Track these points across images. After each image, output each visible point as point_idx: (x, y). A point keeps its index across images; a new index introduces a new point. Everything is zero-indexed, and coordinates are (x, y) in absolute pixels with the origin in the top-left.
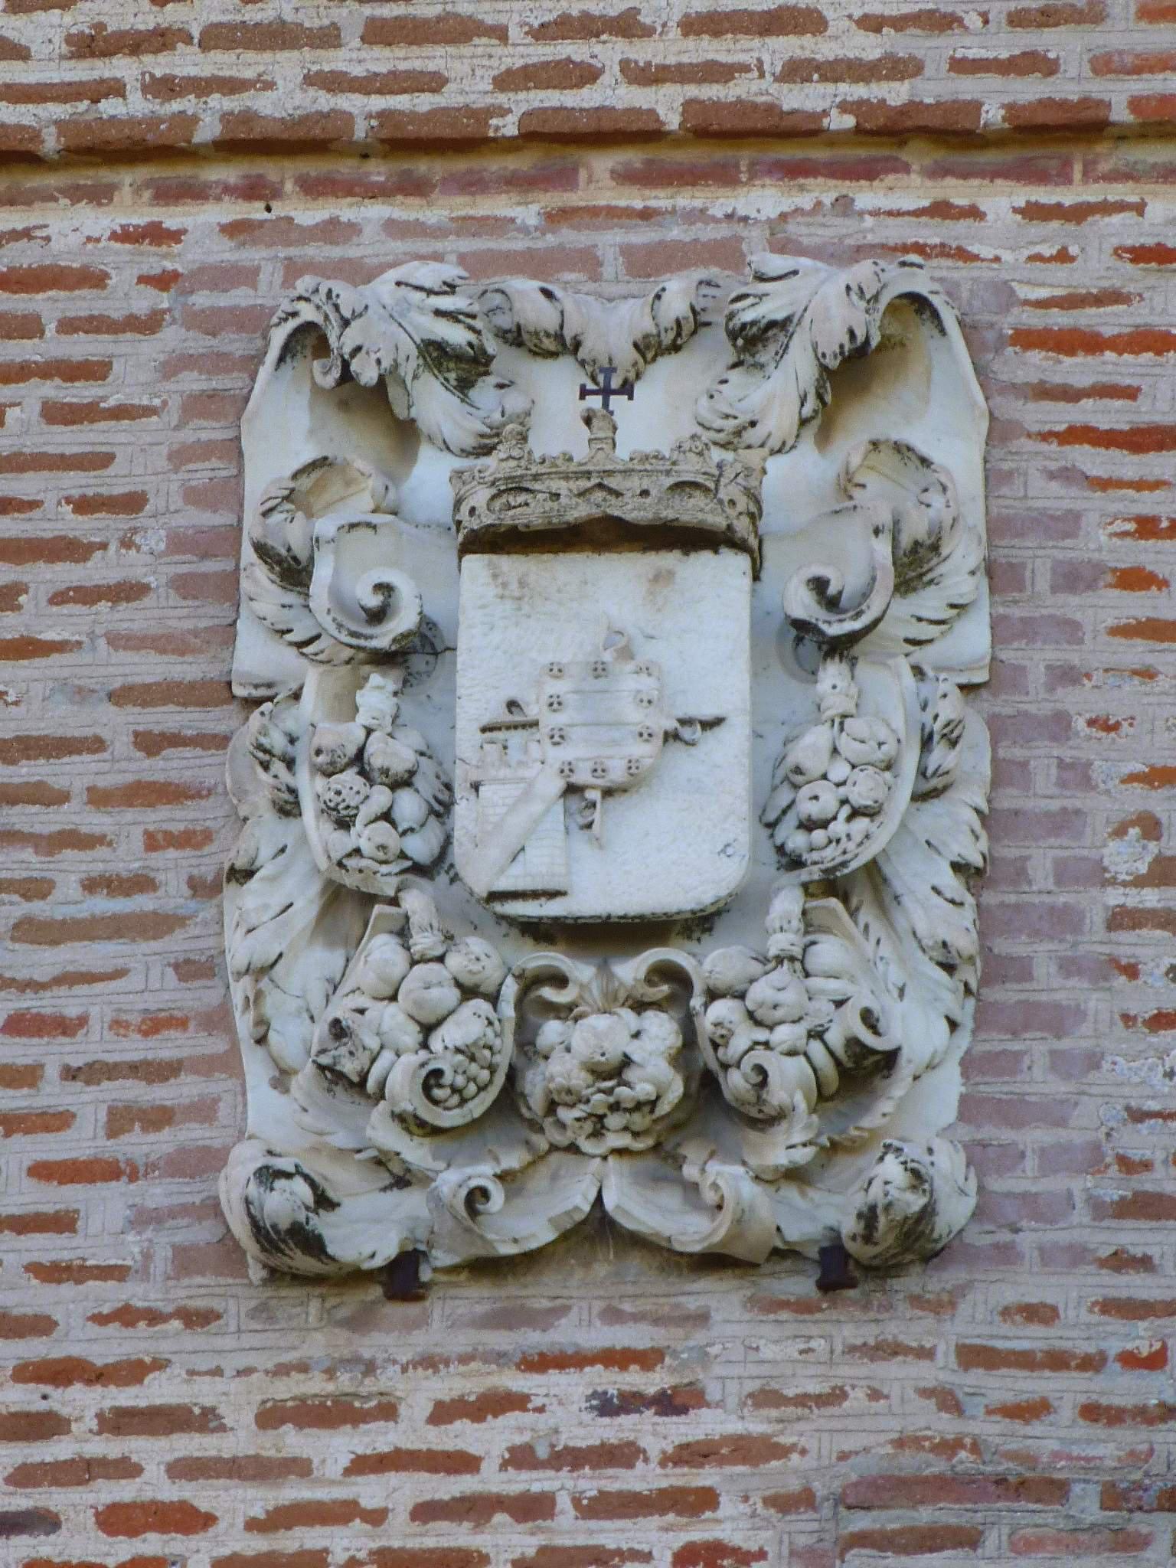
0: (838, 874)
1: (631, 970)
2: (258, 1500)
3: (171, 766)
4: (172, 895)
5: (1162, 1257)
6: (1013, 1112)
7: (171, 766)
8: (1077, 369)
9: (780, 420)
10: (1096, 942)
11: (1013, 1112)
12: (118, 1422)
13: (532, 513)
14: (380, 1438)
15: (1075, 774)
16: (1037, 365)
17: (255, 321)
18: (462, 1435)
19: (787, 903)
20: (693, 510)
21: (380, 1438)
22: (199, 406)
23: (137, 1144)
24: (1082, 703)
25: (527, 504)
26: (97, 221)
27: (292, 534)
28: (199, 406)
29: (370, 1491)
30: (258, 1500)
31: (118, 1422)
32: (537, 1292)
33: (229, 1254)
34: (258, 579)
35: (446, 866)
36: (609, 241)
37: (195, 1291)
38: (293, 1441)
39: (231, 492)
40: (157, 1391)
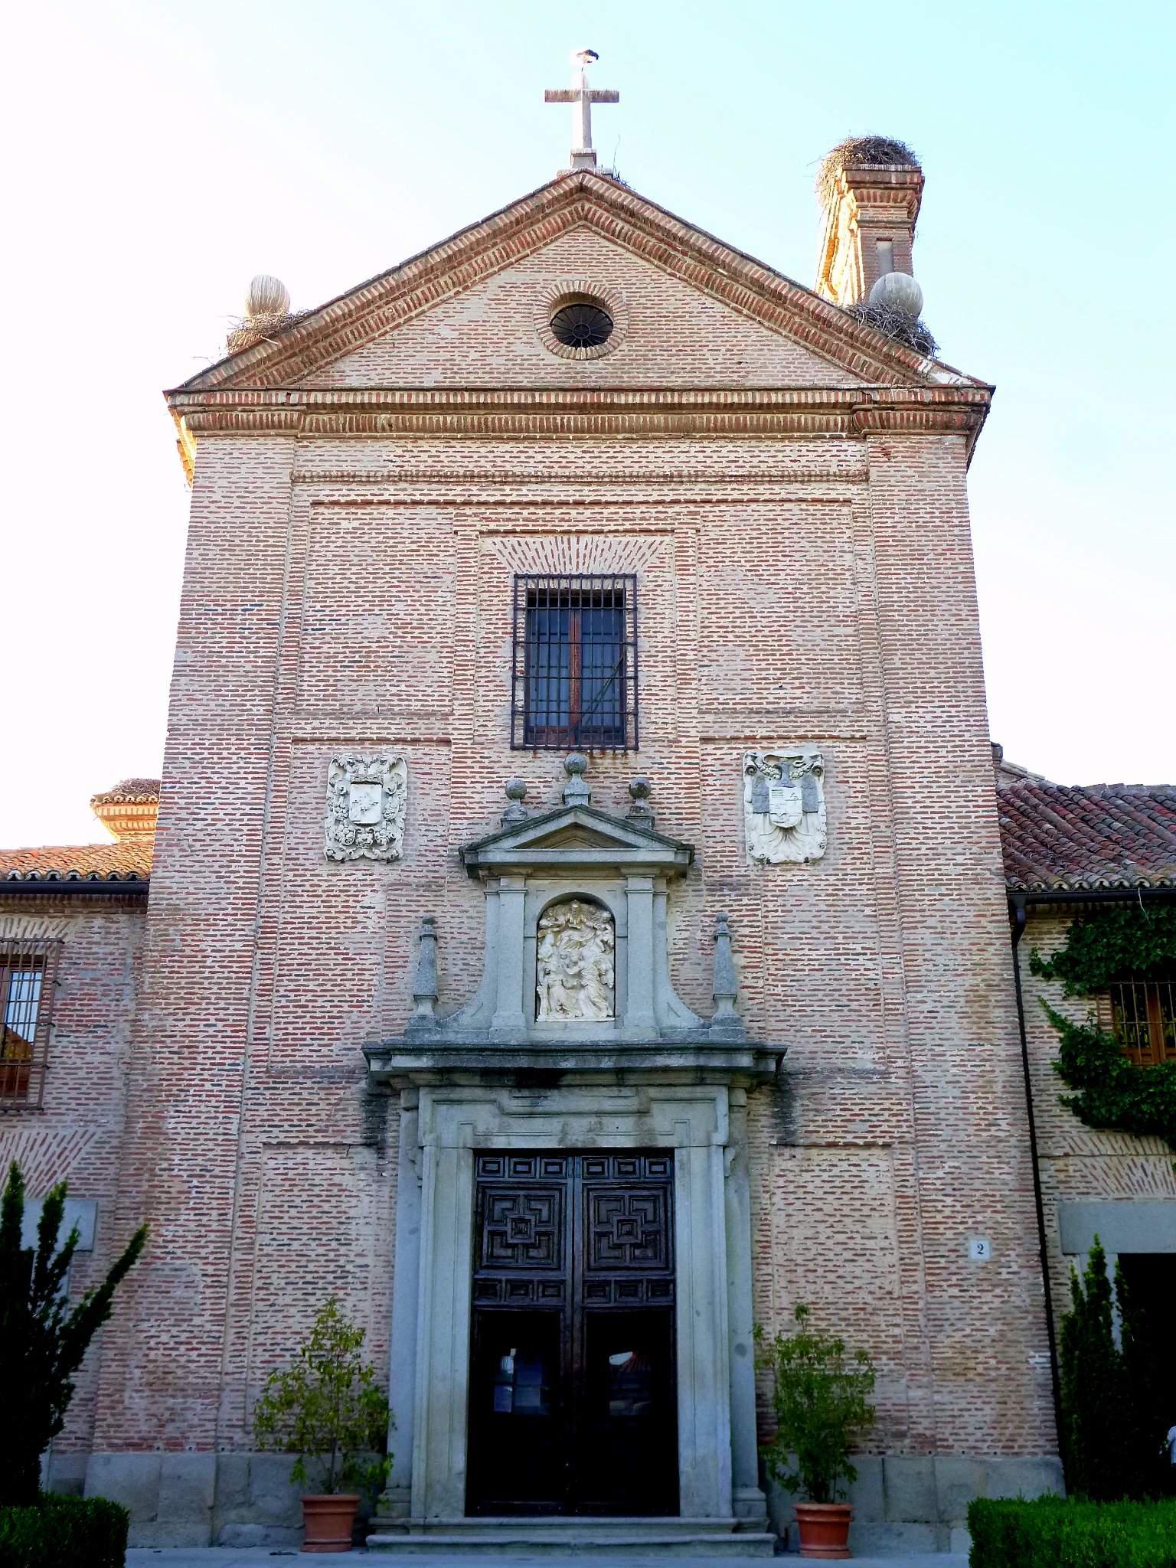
0: (1086, 1299)
1: (368, 829)
2: (327, 884)
3: (319, 806)
4: (319, 820)
5: (356, 802)
6: (407, 845)
7: (319, 806)
8: (417, 766)
9: (385, 771)
10: (417, 827)
11: (407, 845)
12: (312, 875)
13: (358, 780)
14: (339, 878)
15: (415, 809)
16: (413, 766)
17: (330, 758)
18: (348, 878)
19: (384, 823)
20: (375, 780)
21: (339, 878)
22: (324, 767)
23: (315, 846)
24: (416, 801)
25: (864, 477)
26: (314, 747)
27: (333, 782)
28: (324, 767)
29: (338, 883)
30: (327, 884)
31: (312, 875)
32: (357, 863)
33: (324, 858)
34: (329, 786)
35: (265, 318)
36: (368, 751)
37: (321, 862)
38: (330, 878)
39: (327, 777)
40: (316, 872)
